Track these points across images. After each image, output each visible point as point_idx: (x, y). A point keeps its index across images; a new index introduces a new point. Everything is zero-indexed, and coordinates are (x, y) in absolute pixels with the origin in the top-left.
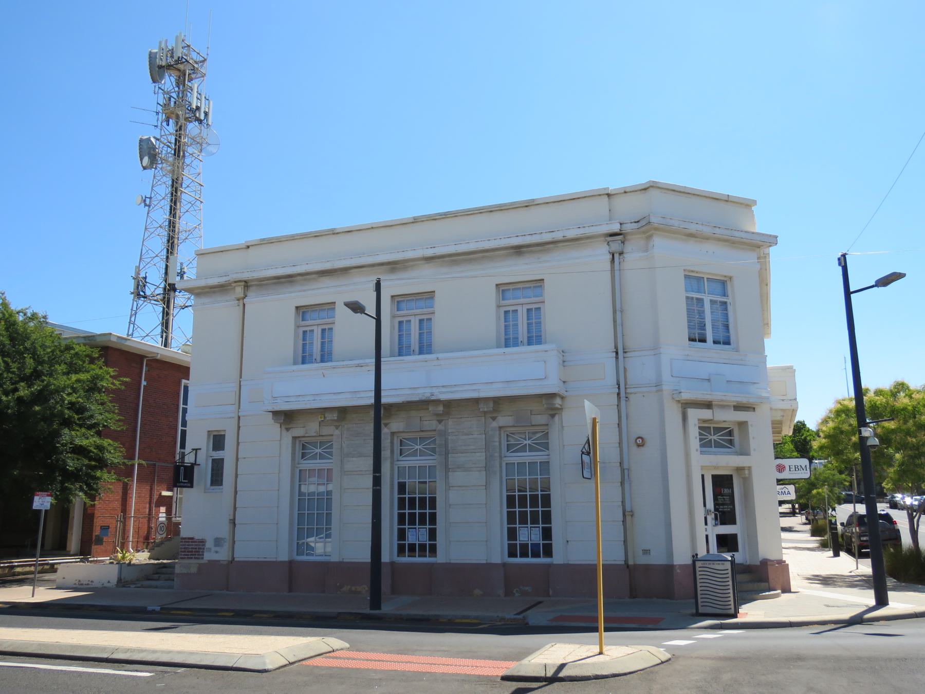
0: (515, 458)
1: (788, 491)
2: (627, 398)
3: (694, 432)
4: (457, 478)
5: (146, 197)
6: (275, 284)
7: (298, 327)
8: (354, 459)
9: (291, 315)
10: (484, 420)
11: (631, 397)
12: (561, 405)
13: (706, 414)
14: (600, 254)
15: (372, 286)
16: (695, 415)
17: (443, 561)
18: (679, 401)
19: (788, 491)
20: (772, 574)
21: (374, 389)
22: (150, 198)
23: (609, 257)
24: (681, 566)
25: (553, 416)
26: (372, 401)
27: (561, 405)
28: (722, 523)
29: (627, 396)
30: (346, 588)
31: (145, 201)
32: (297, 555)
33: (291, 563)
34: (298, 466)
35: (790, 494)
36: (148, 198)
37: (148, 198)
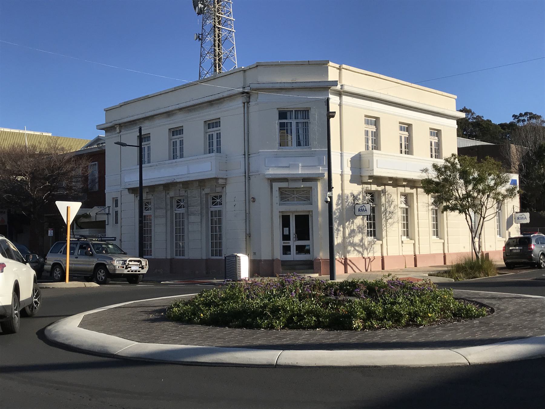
0: (181, 211)
1: (525, 217)
2: (249, 178)
3: (276, 193)
4: (192, 218)
5: (199, 34)
6: (130, 124)
7: (170, 140)
8: (158, 210)
9: (201, 126)
10: (200, 190)
11: (251, 178)
12: (225, 183)
13: (284, 185)
14: (239, 103)
15: (138, 129)
16: (276, 186)
17: (187, 258)
18: (268, 179)
19: (525, 217)
20: (315, 266)
21: (139, 180)
22: (202, 34)
23: (243, 105)
24: (265, 260)
25: (223, 188)
26: (138, 186)
27: (225, 183)
28: (299, 240)
29: (250, 177)
30: (156, 270)
31: (199, 37)
32: (176, 256)
33: (207, 260)
34: (210, 209)
35: (526, 219)
36: (200, 34)
37: (200, 34)
